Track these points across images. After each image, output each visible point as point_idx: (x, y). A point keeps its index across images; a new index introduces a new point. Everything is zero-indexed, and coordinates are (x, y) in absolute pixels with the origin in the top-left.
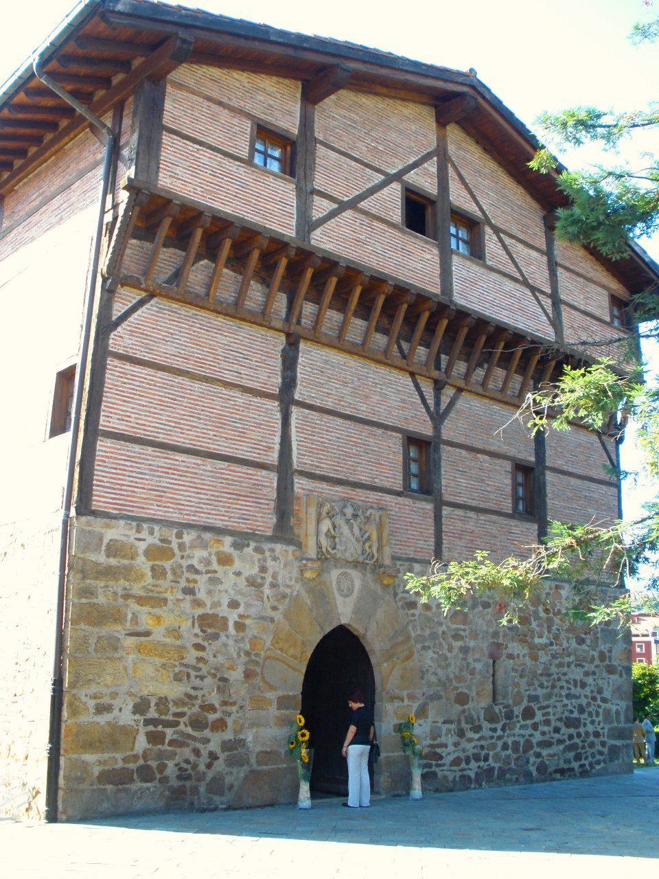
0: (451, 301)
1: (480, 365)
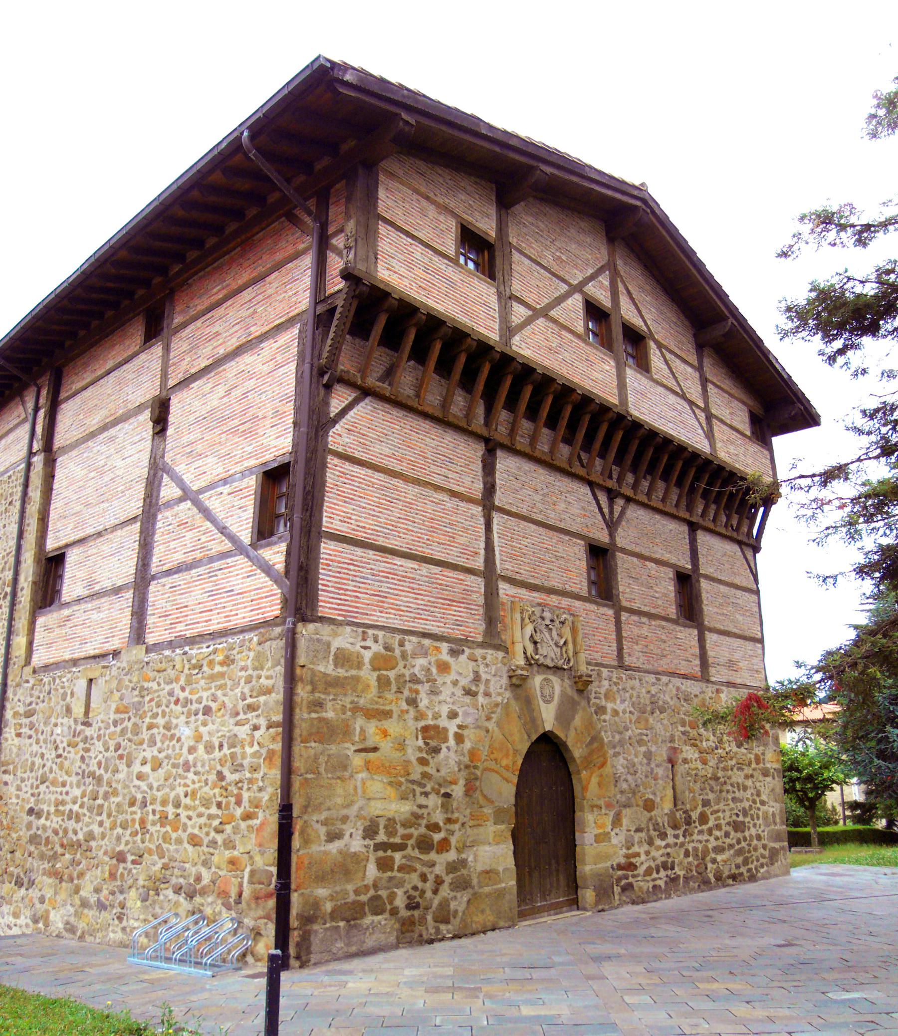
0: (628, 412)
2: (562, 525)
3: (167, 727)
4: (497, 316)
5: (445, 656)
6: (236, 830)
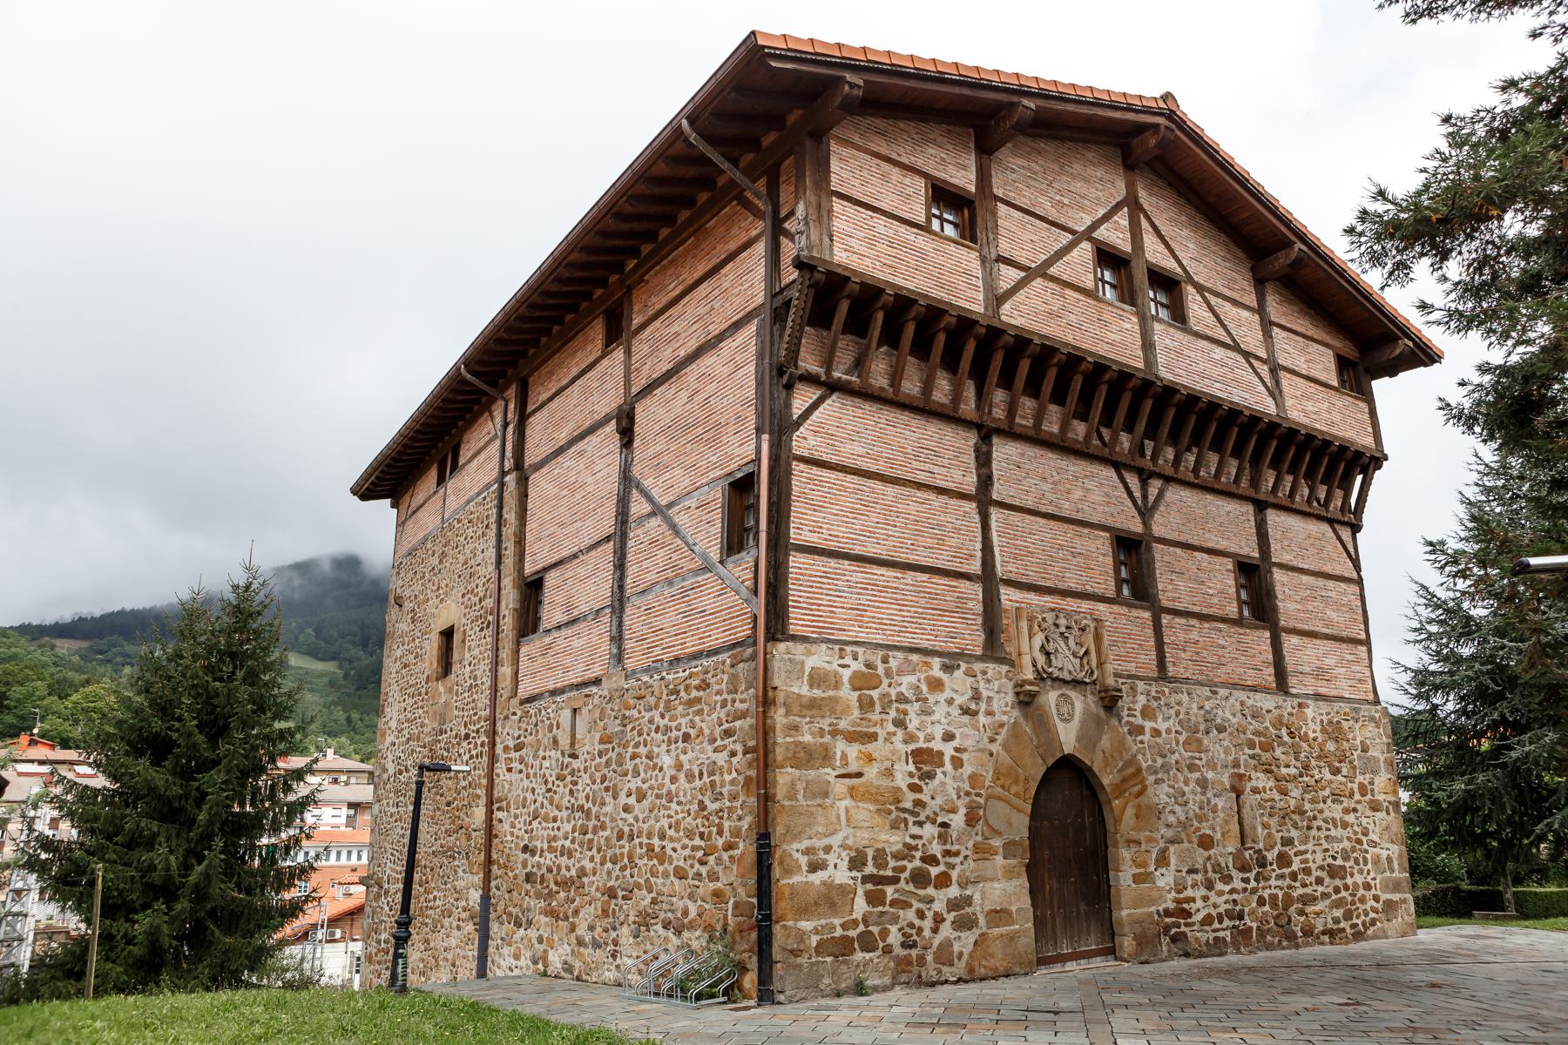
0: (1157, 377)
1: (1189, 449)
2: (1079, 517)
3: (649, 757)
4: (980, 284)
5: (936, 671)
6: (719, 861)
